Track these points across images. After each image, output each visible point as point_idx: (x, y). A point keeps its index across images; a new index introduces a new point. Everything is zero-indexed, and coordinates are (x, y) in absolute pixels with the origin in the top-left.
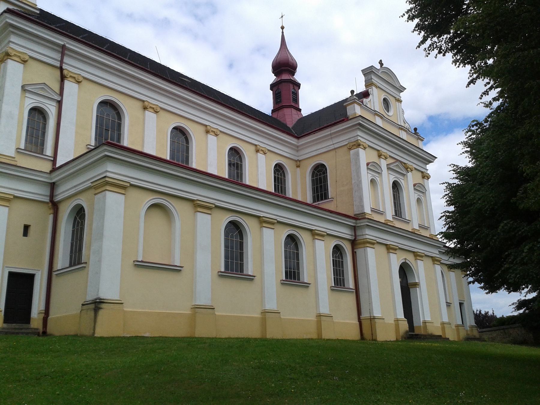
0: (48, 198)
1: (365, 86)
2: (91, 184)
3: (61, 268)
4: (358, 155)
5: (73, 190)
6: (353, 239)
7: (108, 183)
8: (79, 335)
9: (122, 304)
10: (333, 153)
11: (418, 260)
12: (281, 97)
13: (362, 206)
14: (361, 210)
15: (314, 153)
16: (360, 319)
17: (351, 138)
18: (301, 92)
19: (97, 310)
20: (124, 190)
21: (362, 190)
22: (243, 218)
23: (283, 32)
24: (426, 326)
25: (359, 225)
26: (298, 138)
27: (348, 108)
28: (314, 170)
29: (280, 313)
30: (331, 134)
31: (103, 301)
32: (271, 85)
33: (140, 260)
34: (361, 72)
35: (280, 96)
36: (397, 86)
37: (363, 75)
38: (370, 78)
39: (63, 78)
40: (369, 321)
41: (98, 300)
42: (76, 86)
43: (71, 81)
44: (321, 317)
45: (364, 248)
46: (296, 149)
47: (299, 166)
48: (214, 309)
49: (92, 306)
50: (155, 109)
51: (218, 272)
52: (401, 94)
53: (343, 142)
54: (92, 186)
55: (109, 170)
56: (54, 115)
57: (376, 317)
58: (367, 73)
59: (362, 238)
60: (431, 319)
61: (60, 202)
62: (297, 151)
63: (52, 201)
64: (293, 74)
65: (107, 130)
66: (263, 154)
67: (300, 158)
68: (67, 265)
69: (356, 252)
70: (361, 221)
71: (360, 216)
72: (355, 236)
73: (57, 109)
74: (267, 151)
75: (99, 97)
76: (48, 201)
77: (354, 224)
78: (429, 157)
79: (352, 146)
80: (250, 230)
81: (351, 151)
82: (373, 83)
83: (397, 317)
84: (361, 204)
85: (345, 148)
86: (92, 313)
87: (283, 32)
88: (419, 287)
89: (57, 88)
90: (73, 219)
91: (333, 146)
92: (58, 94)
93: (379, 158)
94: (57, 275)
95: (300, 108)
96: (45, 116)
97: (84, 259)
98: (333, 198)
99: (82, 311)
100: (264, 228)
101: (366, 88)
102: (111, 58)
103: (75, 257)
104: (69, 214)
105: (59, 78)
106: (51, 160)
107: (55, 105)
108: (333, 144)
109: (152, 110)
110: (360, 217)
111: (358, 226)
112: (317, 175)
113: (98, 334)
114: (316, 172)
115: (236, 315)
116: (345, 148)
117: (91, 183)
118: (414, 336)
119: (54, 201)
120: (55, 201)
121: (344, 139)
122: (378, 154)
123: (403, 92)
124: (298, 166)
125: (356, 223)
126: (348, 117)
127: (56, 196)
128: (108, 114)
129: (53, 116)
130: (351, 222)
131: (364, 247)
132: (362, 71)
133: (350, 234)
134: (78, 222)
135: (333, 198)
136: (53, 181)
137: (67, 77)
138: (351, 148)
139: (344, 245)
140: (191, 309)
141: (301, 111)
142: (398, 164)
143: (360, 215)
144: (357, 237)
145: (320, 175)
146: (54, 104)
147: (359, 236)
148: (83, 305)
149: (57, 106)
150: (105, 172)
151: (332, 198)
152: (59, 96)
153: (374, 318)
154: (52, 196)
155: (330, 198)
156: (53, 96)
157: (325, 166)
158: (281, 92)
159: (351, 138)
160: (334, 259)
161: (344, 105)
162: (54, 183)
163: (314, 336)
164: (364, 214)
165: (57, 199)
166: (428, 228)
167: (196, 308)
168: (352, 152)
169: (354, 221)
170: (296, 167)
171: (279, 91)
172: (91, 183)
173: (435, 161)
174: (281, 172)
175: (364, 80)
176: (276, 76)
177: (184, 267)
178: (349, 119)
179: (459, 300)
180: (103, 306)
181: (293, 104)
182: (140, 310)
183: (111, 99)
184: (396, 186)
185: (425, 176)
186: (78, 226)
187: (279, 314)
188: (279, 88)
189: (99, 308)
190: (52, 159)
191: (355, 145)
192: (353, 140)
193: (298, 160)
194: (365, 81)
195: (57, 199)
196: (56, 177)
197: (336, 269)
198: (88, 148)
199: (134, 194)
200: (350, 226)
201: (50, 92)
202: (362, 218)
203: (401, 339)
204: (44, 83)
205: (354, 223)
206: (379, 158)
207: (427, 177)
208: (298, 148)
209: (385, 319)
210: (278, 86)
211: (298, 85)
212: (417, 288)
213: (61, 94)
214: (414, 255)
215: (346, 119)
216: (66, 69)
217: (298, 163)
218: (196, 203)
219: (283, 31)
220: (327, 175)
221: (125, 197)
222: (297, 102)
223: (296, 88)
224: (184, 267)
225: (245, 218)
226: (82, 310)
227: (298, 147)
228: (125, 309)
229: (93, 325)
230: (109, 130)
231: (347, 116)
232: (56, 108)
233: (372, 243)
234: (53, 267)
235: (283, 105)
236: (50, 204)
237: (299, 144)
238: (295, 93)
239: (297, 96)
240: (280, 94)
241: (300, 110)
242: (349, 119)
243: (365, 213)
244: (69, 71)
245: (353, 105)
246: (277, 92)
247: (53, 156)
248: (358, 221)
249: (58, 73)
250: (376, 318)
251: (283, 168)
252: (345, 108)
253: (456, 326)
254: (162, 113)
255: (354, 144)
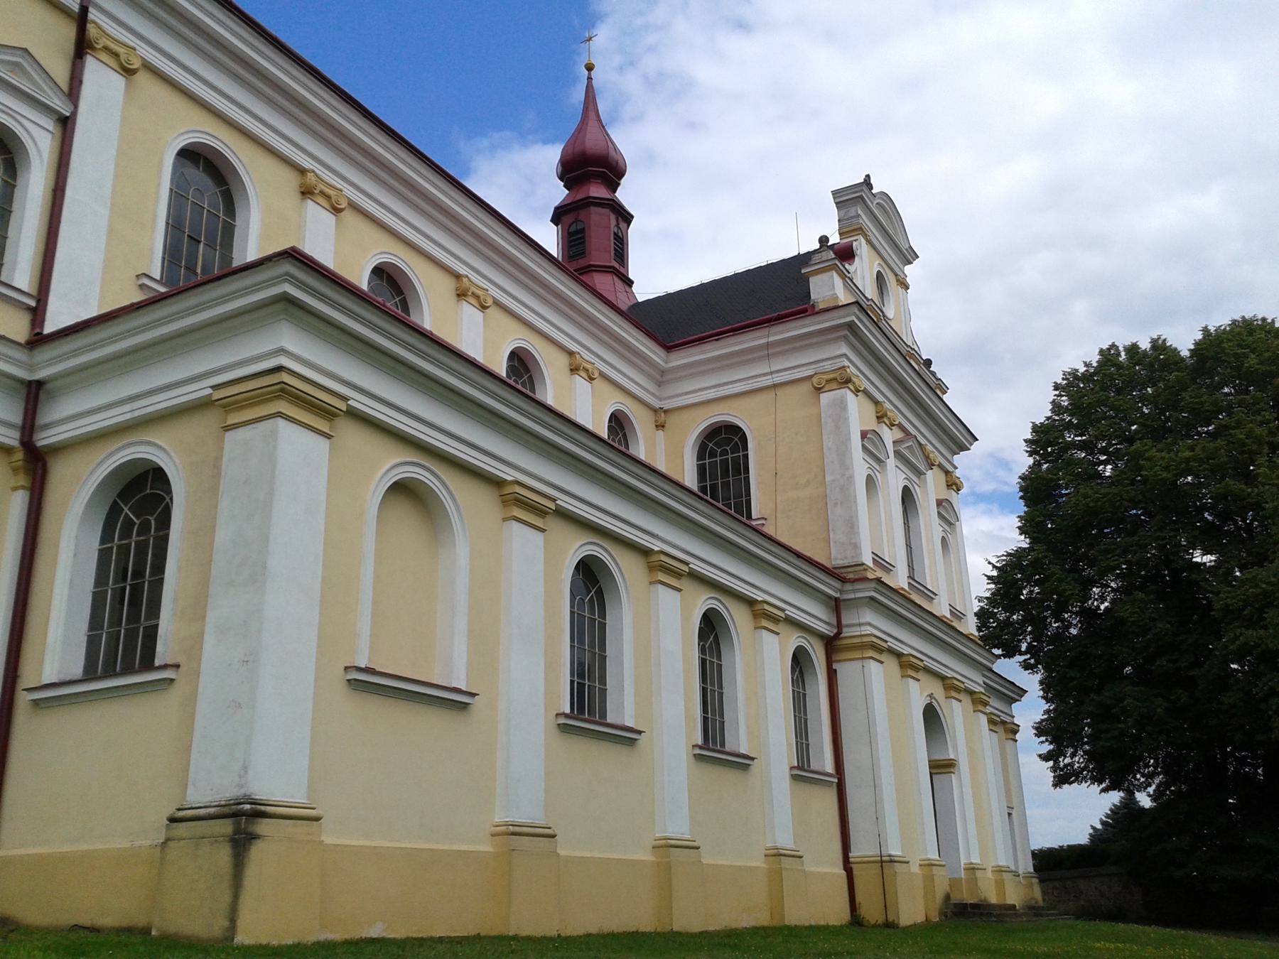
0: (17, 435)
1: (840, 234)
2: (210, 391)
3: (54, 680)
4: (843, 405)
5: (127, 407)
6: (832, 635)
7: (285, 393)
8: (154, 933)
9: (317, 819)
10: (769, 396)
11: (953, 700)
12: (584, 242)
13: (856, 547)
14: (853, 557)
15: (712, 394)
16: (849, 862)
17: (823, 360)
18: (634, 233)
19: (242, 842)
20: (328, 423)
21: (855, 502)
22: (612, 552)
23: (590, 78)
24: (976, 878)
25: (852, 596)
26: (669, 348)
27: (811, 279)
28: (704, 438)
29: (697, 848)
30: (768, 345)
31: (263, 808)
32: (557, 209)
33: (364, 666)
34: (831, 196)
35: (582, 240)
36: (904, 246)
37: (835, 205)
38: (852, 215)
39: (83, 47)
40: (875, 870)
41: (248, 807)
42: (118, 81)
43: (104, 63)
44: (780, 860)
45: (861, 661)
46: (658, 377)
47: (663, 426)
48: (553, 836)
49: (226, 827)
50: (333, 198)
51: (557, 715)
52: (906, 267)
53: (799, 370)
54: (214, 398)
55: (290, 347)
56: (46, 155)
57: (896, 859)
58: (847, 200)
59: (859, 633)
60: (902, 851)
61: (58, 449)
62: (660, 384)
63: (27, 444)
64: (614, 186)
65: (195, 240)
66: (586, 378)
67: (667, 405)
68: (77, 670)
69: (835, 671)
70: (858, 586)
71: (851, 572)
72: (839, 625)
73: (57, 144)
74: (596, 375)
75: (182, 131)
76: (16, 443)
77: (837, 592)
78: (963, 436)
79: (827, 381)
80: (626, 587)
81: (821, 395)
82: (861, 228)
83: (888, 851)
84: (853, 541)
85: (806, 388)
86: (224, 855)
87: (590, 78)
88: (956, 773)
89: (60, 72)
90: (108, 508)
91: (770, 377)
92: (64, 93)
93: (879, 423)
94: (36, 703)
95: (631, 276)
96: (12, 159)
97: (163, 653)
98: (766, 519)
99: (171, 844)
100: (660, 586)
101: (841, 239)
102: (229, 17)
103: (114, 638)
104: (94, 495)
105: (70, 47)
106: (29, 308)
107: (51, 129)
108: (771, 373)
109: (325, 201)
110: (851, 576)
111: (845, 600)
112: (713, 455)
113: (242, 938)
114: (711, 445)
115: (597, 855)
116: (806, 388)
117: (212, 387)
118: (969, 909)
119: (35, 446)
120: (39, 444)
121: (803, 362)
122: (877, 412)
123: (912, 265)
124: (660, 426)
125: (841, 592)
126: (813, 306)
127: (47, 426)
128: (198, 189)
129: (42, 161)
130: (830, 588)
131: (863, 658)
132: (835, 193)
133: (827, 620)
134: (129, 524)
135: (766, 519)
136: (40, 375)
137: (96, 45)
138: (823, 387)
139: (813, 648)
140: (492, 835)
141: (631, 287)
142: (911, 443)
143: (850, 570)
144: (844, 630)
145: (725, 453)
146: (49, 124)
147: (849, 626)
148: (173, 820)
149: (58, 134)
150: (277, 352)
151: (763, 518)
152: (64, 98)
153: (891, 861)
154: (29, 427)
155: (756, 517)
156: (49, 96)
157: (742, 430)
158: (584, 229)
159: (823, 360)
160: (795, 689)
161: (803, 272)
162: (40, 384)
163: (761, 918)
164: (861, 568)
165: (44, 439)
166: (962, 616)
167: (514, 832)
168: (825, 397)
169: (837, 584)
170: (654, 427)
171: (580, 227)
172: (215, 387)
173: (973, 446)
174: (620, 435)
175: (837, 219)
176: (568, 189)
177: (478, 695)
178: (817, 309)
179: (1008, 807)
180: (264, 827)
181: (617, 265)
182: (361, 843)
183: (212, 144)
184: (907, 497)
185: (954, 485)
186: (126, 533)
187: (696, 850)
188: (580, 218)
189: (251, 834)
190: (33, 303)
191: (835, 379)
192: (828, 366)
193: (661, 408)
194: (839, 221)
195: (44, 439)
196: (47, 366)
197: (708, 714)
198: (142, 286)
199: (353, 437)
200: (825, 598)
201: (41, 82)
202: (856, 577)
203: (938, 919)
204: (26, 50)
205: (836, 590)
206: (879, 423)
207: (956, 484)
208: (662, 376)
209: (910, 863)
210: (578, 214)
211: (626, 217)
212: (953, 775)
213: (73, 91)
214: (943, 685)
215: (802, 307)
216: (94, 22)
217: (661, 418)
218: (508, 490)
219: (589, 74)
220: (746, 457)
221: (330, 444)
222: (623, 260)
223: (623, 225)
224: (478, 695)
225: (617, 552)
226: (168, 840)
227: (663, 372)
228: (328, 840)
229: (227, 898)
230: (199, 242)
231: (812, 303)
232: (52, 138)
233: (878, 648)
234: (18, 673)
235: (592, 263)
236: (19, 456)
237: (666, 366)
238: (620, 238)
239: (623, 246)
240: (583, 235)
241: (630, 283)
242: (817, 309)
243: (863, 564)
244: (104, 31)
245: (828, 274)
246: (573, 229)
247: (34, 292)
248: (848, 587)
249: (68, 32)
250: (895, 862)
251: (625, 428)
252: (805, 281)
253: (925, 865)
254: (349, 216)
255: (832, 376)
